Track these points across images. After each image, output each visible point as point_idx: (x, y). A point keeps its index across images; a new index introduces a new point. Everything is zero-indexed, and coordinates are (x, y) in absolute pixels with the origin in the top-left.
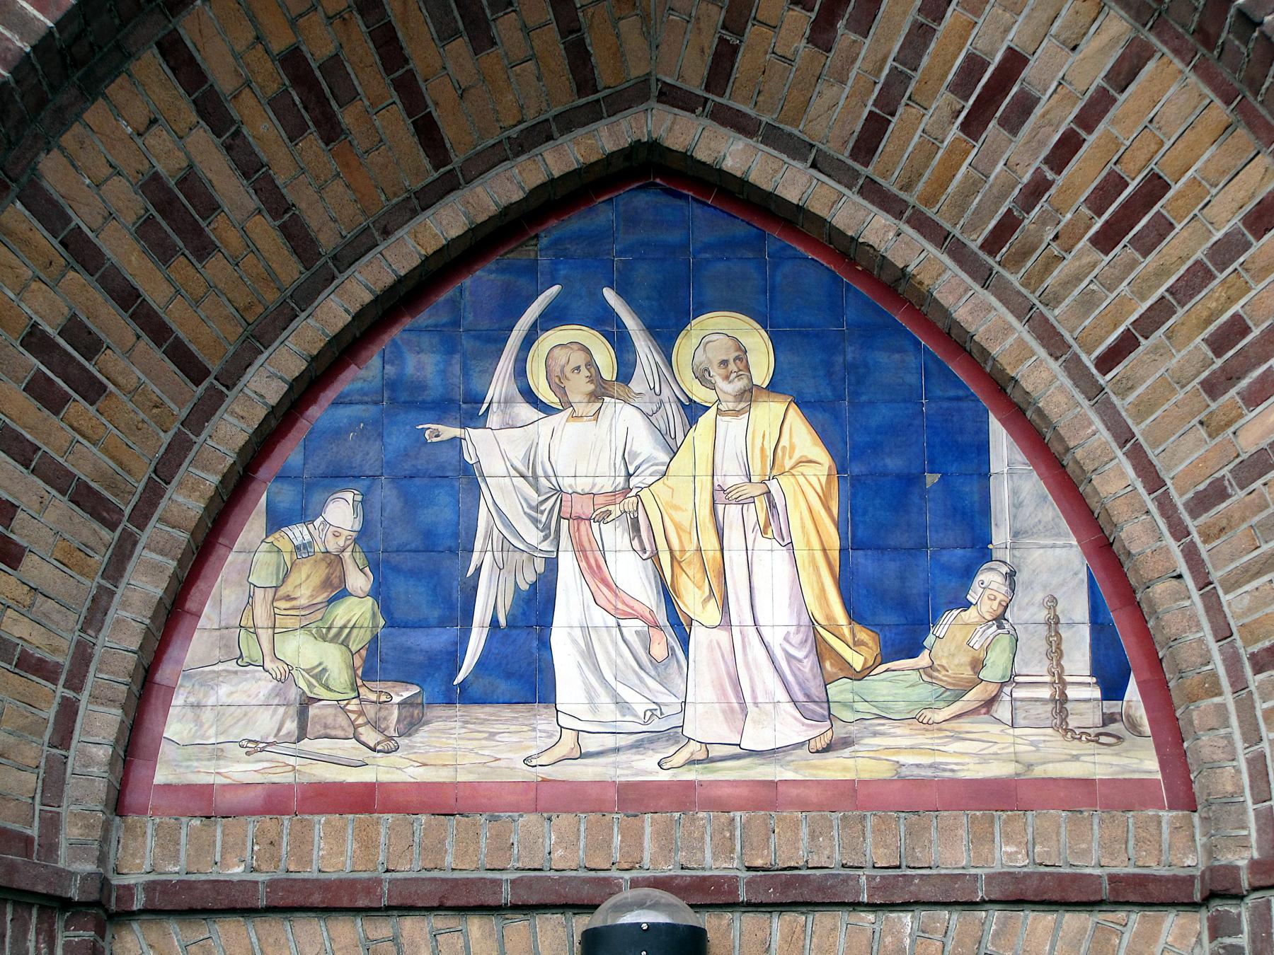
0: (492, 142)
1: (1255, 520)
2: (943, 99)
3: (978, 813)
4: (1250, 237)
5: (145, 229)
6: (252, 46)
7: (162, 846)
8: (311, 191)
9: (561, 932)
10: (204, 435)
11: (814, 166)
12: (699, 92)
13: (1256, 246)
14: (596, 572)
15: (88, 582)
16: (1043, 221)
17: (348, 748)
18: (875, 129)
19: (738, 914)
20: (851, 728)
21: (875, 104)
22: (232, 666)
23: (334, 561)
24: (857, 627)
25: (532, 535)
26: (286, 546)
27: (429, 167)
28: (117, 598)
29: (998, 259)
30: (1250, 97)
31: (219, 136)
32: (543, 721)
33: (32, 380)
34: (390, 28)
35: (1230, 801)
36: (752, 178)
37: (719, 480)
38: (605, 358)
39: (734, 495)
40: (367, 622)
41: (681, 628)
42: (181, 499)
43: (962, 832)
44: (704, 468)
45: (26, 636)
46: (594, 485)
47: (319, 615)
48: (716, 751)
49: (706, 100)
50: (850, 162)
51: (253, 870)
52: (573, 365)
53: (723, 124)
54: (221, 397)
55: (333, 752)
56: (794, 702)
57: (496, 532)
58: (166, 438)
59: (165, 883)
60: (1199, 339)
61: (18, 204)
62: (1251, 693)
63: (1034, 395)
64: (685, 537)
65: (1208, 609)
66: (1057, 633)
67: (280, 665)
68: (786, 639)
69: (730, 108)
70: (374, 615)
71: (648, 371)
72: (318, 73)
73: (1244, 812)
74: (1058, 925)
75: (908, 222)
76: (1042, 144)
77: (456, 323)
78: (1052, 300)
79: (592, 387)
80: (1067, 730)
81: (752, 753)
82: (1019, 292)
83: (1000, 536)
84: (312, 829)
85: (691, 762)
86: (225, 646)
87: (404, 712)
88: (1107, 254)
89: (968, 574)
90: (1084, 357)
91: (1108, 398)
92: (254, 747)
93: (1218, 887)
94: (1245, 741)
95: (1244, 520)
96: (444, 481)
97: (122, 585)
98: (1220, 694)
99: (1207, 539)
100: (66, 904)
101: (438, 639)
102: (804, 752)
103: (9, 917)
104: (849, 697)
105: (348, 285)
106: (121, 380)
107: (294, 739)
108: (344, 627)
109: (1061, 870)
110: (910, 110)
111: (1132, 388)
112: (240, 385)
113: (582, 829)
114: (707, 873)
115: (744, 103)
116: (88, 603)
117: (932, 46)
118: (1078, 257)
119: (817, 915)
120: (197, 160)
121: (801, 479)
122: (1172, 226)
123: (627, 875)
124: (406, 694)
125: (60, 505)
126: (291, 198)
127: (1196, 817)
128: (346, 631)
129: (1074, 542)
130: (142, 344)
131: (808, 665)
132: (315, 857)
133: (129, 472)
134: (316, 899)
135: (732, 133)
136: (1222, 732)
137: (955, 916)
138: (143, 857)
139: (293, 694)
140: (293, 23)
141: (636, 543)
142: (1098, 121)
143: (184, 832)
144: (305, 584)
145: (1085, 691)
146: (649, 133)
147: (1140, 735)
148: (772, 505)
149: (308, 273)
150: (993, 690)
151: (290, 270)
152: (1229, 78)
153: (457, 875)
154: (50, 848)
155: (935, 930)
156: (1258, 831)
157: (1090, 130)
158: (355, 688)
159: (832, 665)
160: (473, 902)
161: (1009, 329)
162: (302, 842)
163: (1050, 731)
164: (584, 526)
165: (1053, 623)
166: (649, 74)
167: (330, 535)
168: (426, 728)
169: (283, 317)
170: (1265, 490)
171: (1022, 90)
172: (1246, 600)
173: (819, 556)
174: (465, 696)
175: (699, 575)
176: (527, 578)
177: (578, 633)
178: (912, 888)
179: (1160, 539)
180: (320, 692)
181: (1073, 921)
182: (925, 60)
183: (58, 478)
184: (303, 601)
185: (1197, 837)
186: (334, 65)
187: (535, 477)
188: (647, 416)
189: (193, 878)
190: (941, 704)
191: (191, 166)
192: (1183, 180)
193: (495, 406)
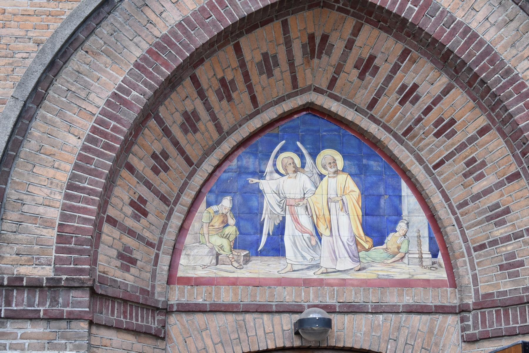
0: (269, 101)
1: (476, 211)
2: (394, 95)
3: (400, 288)
4: (478, 137)
5: (182, 126)
6: (213, 77)
7: (180, 294)
8: (223, 115)
9: (288, 319)
10: (191, 181)
11: (356, 110)
12: (325, 89)
13: (480, 139)
14: (296, 221)
15: (162, 221)
16: (420, 129)
18: (374, 102)
19: (336, 315)
20: (366, 265)
21: (375, 95)
22: (198, 244)
23: (225, 216)
24: (367, 237)
25: (279, 210)
26: (212, 212)
27: (253, 108)
28: (169, 225)
29: (406, 138)
30: (481, 100)
31: (202, 100)
32: (282, 261)
33: (153, 167)
34: (247, 72)
35: (467, 286)
36: (339, 113)
37: (329, 196)
38: (298, 161)
39: (333, 200)
40: (234, 233)
41: (319, 236)
42: (185, 198)
43: (395, 293)
44: (325, 192)
45: (148, 236)
46: (295, 196)
47: (221, 231)
48: (329, 270)
49: (327, 91)
50: (366, 110)
51: (205, 300)
52: (289, 163)
53: (331, 98)
54: (196, 170)
55: (226, 269)
56: (350, 257)
57: (269, 209)
58: (182, 182)
59: (182, 304)
60: (462, 162)
61: (153, 119)
62: (473, 257)
63: (415, 175)
64: (320, 211)
65: (461, 235)
66: (420, 240)
67: (211, 244)
68: (348, 240)
69: (333, 94)
70: (236, 231)
71: (309, 165)
72: (228, 84)
73: (471, 289)
74: (421, 319)
75: (381, 127)
76: (421, 108)
77: (257, 151)
78: (421, 150)
79: (294, 169)
80: (423, 266)
81: (339, 271)
82: (412, 147)
83: (405, 213)
84: (221, 290)
85: (322, 273)
86: (196, 239)
87: (245, 258)
88: (437, 138)
89: (396, 223)
90: (429, 165)
91: (435, 177)
92: (204, 267)
93: (464, 309)
94: (471, 270)
95: (473, 211)
96: (254, 194)
97: (170, 222)
98: (464, 257)
99: (462, 215)
100: (158, 309)
101: (254, 238)
102: (353, 271)
103: (145, 312)
104: (365, 256)
105: (229, 140)
106: (173, 166)
107: (215, 265)
108: (228, 234)
109: (422, 304)
110: (385, 97)
111: (442, 174)
112: (201, 167)
113: (294, 291)
114: (328, 304)
115: (338, 93)
116: (162, 227)
117: (393, 81)
118: (429, 139)
119: (357, 315)
120: (196, 107)
121: (351, 196)
122: (456, 132)
123: (306, 304)
124: (245, 253)
125: (157, 200)
126: (218, 117)
127: (457, 290)
128: (228, 235)
129: (424, 215)
130: (179, 156)
131: (354, 247)
132: (221, 297)
133: (173, 191)
135: (332, 100)
136: (465, 267)
137: (394, 316)
138: (175, 296)
139: (215, 252)
140: (223, 71)
141: (307, 212)
142: (438, 103)
143: (186, 290)
144: (217, 222)
145: (427, 255)
146: (311, 100)
147: (442, 267)
148: (344, 203)
149: (220, 137)
150: (403, 255)
151: (216, 136)
152: (475, 95)
153: (260, 303)
154: (153, 294)
155: (388, 320)
156: (474, 294)
157: (435, 106)
158: (231, 251)
159: (360, 247)
160: (265, 310)
161: (408, 157)
162: (218, 293)
163: (418, 266)
164: (293, 207)
165: (419, 237)
166: (312, 84)
167: (223, 208)
168: (251, 262)
169: (213, 148)
170: (479, 203)
171: (417, 94)
172: (473, 232)
173: (356, 217)
175: (324, 222)
176: (277, 222)
177: (291, 237)
178: (383, 308)
179: (449, 215)
180: (222, 252)
181: (425, 317)
182: (390, 85)
183: (157, 193)
184: (217, 227)
185: (457, 295)
186: (232, 81)
187: (279, 194)
188: (309, 177)
189: (189, 302)
190: (389, 258)
191: (195, 109)
192: (460, 120)
193: (268, 174)
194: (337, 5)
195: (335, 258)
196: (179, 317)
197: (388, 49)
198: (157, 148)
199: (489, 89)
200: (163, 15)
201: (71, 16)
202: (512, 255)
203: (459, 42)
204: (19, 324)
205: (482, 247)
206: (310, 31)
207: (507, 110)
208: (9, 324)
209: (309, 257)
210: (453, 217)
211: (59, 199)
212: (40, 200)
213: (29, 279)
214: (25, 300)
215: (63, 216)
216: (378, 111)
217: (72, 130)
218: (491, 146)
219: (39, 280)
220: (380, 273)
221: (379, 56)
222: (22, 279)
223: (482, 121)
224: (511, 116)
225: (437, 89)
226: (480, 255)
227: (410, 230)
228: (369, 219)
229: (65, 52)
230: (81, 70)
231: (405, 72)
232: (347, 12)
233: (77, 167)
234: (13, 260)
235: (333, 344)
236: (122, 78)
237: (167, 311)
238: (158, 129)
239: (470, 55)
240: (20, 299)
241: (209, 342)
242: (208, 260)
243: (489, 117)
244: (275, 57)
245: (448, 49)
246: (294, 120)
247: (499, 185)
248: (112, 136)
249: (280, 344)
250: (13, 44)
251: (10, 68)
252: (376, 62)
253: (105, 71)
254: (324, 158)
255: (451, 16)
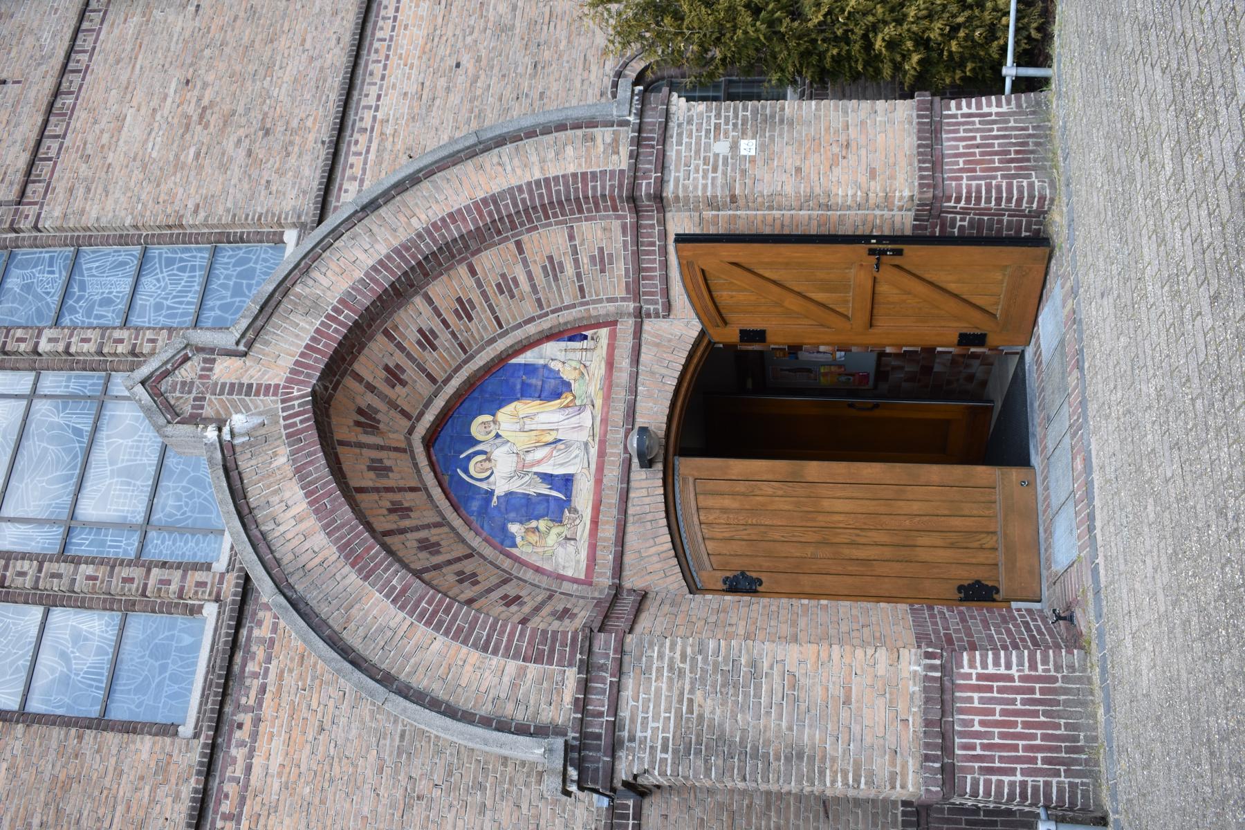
2: (426, 354)
14: (539, 462)
17: (580, 528)
25: (527, 478)
32: (578, 477)
41: (557, 441)
44: (514, 434)
89: (551, 370)
92: (577, 552)
99: (550, 306)
131: (570, 410)
134: (621, 535)
135: (423, 419)
144: (533, 538)
162: (605, 540)
174: (569, 500)
176: (539, 480)
180: (564, 535)
181: (644, 349)
186: (393, 503)
194: (330, 391)
195: (580, 427)
196: (626, 579)
197: (380, 350)
198: (452, 578)
199: (433, 253)
200: (317, 550)
201: (304, 641)
202: (593, 258)
203: (385, 276)
204: (623, 703)
205: (581, 289)
206: (352, 424)
207: (456, 239)
208: (622, 714)
209: (577, 452)
210: (551, 316)
211: (495, 661)
212: (496, 680)
213: (578, 691)
214: (598, 697)
215: (515, 657)
216: (440, 375)
217: (425, 646)
218: (487, 266)
219: (579, 681)
220: (598, 386)
221: (386, 360)
222: (577, 699)
223: (462, 270)
224: (462, 237)
225: (426, 310)
226: (589, 292)
227: (559, 358)
228: (543, 395)
229: (342, 650)
230: (363, 634)
231: (405, 338)
232: (338, 383)
233: (465, 642)
234: (556, 709)
235: (663, 433)
236: (378, 594)
237: (618, 589)
238: (433, 573)
239: (399, 267)
240: (597, 703)
241: (653, 550)
242: (570, 547)
243: (460, 262)
244: (373, 460)
245: (390, 286)
246: (438, 461)
247: (525, 262)
248: (436, 606)
249: (660, 482)
250: (319, 757)
251: (344, 761)
252: (391, 365)
253: (368, 611)
254: (480, 432)
255: (358, 281)
